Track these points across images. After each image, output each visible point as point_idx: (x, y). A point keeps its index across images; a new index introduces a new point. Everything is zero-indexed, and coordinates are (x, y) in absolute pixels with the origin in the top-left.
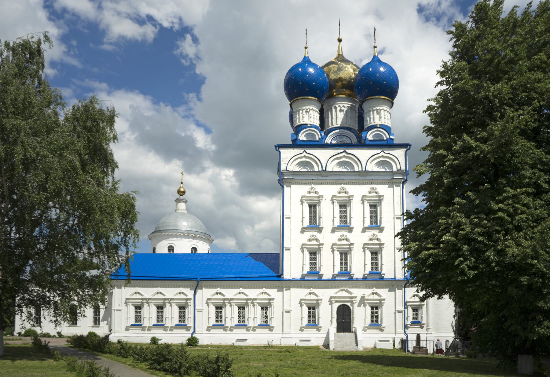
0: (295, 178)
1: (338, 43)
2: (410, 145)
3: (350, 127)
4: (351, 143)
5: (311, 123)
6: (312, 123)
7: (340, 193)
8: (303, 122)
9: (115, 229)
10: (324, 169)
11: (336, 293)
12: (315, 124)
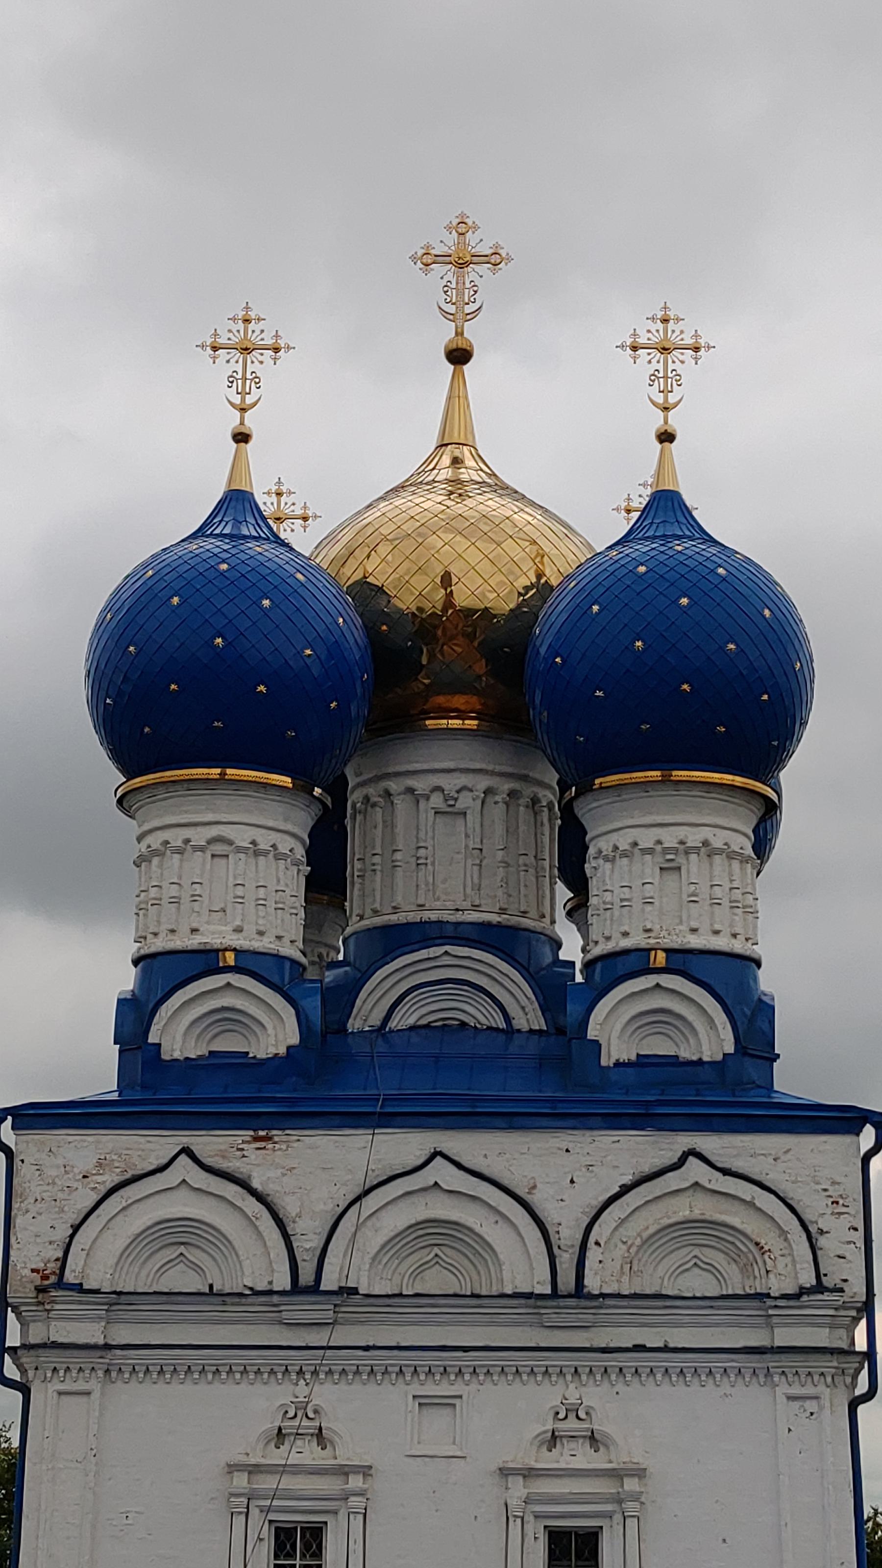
10: (306, 1277)
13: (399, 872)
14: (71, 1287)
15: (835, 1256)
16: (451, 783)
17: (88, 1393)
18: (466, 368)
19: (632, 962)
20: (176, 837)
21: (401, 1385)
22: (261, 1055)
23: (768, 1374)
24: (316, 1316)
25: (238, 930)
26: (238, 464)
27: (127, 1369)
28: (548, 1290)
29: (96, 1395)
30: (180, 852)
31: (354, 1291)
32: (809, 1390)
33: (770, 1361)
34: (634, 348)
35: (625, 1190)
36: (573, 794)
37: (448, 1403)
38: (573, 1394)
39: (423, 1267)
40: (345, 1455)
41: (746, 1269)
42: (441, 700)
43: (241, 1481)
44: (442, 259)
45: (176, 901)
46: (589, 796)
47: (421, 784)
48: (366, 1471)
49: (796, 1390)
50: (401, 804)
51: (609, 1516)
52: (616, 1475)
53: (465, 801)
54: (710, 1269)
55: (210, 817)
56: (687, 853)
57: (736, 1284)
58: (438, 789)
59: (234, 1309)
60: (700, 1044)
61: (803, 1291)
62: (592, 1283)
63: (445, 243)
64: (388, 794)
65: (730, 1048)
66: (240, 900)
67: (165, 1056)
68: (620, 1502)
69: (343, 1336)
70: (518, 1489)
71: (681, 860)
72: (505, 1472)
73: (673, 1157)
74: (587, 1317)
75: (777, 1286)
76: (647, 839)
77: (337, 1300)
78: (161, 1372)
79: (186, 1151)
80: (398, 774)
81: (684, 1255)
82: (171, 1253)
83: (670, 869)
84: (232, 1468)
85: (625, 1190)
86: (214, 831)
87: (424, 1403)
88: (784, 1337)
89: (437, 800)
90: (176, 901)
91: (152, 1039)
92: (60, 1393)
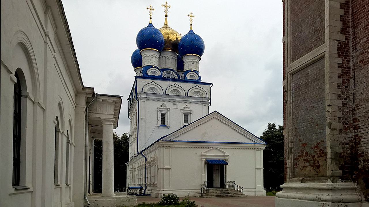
1: (165, 17)
13: (164, 64)
16: (169, 56)
17: (144, 101)
18: (167, 17)
19: (190, 71)
20: (146, 55)
22: (157, 76)
24: (165, 96)
26: (166, 20)
29: (145, 102)
35: (191, 88)
36: (108, 101)
37: (176, 104)
39: (174, 93)
41: (201, 95)
43: (159, 109)
47: (166, 56)
50: (164, 58)
52: (190, 110)
53: (170, 58)
54: (198, 95)
55: (151, 53)
58: (168, 57)
59: (158, 95)
61: (206, 97)
63: (165, 4)
64: (162, 57)
70: (182, 111)
72: (181, 110)
74: (188, 98)
76: (191, 60)
84: (158, 108)
85: (191, 88)
87: (174, 104)
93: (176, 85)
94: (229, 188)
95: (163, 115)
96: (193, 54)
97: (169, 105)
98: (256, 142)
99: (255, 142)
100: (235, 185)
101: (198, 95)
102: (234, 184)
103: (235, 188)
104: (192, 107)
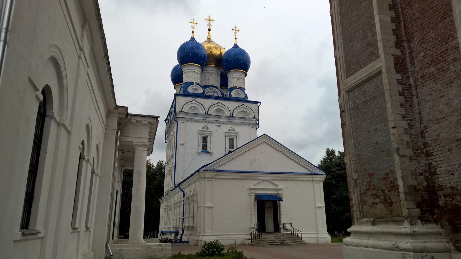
0: (188, 117)
1: (208, 31)
2: (260, 103)
3: (216, 86)
4: (217, 96)
5: (196, 82)
6: (197, 82)
7: (229, 130)
8: (206, 84)
9: (451, 115)
10: (206, 113)
11: (255, 185)
12: (198, 82)
14: (183, 112)
15: (113, 240)
16: (212, 72)
17: (184, 123)
18: (210, 31)
21: (215, 124)
23: (250, 125)
25: (196, 81)
27: (188, 121)
28: (230, 116)
29: (185, 123)
30: (190, 72)
31: (211, 115)
32: (253, 127)
33: (250, 124)
34: (233, 30)
37: (220, 126)
38: (232, 126)
39: (217, 113)
40: (210, 130)
42: (211, 63)
43: (200, 132)
44: (208, 20)
45: (189, 77)
46: (230, 72)
47: (209, 72)
48: (212, 131)
49: (252, 127)
50: (206, 74)
51: (235, 137)
52: (236, 133)
53: (213, 74)
54: (244, 116)
56: (240, 78)
57: (246, 116)
58: (211, 72)
60: (241, 96)
61: (253, 118)
62: (234, 115)
63: (208, 18)
65: (244, 97)
66: (196, 78)
67: (189, 92)
68: (236, 136)
69: (210, 119)
70: (227, 134)
71: (240, 79)
73: (241, 105)
75: (251, 117)
76: (236, 76)
77: (210, 115)
78: (192, 121)
79: (194, 100)
80: (207, 70)
81: (242, 114)
82: (192, 110)
83: (238, 80)
84: (199, 130)
86: (194, 70)
87: (217, 126)
88: (251, 122)
89: (210, 73)
90: (189, 77)
91: (188, 90)
92: (181, 122)
93: (219, 104)
94: (285, 232)
95: (205, 140)
96: (238, 70)
97: (212, 127)
98: (314, 172)
99: (312, 172)
100: (292, 228)
101: (195, 112)
102: (291, 226)
103: (292, 233)
104: (238, 129)
